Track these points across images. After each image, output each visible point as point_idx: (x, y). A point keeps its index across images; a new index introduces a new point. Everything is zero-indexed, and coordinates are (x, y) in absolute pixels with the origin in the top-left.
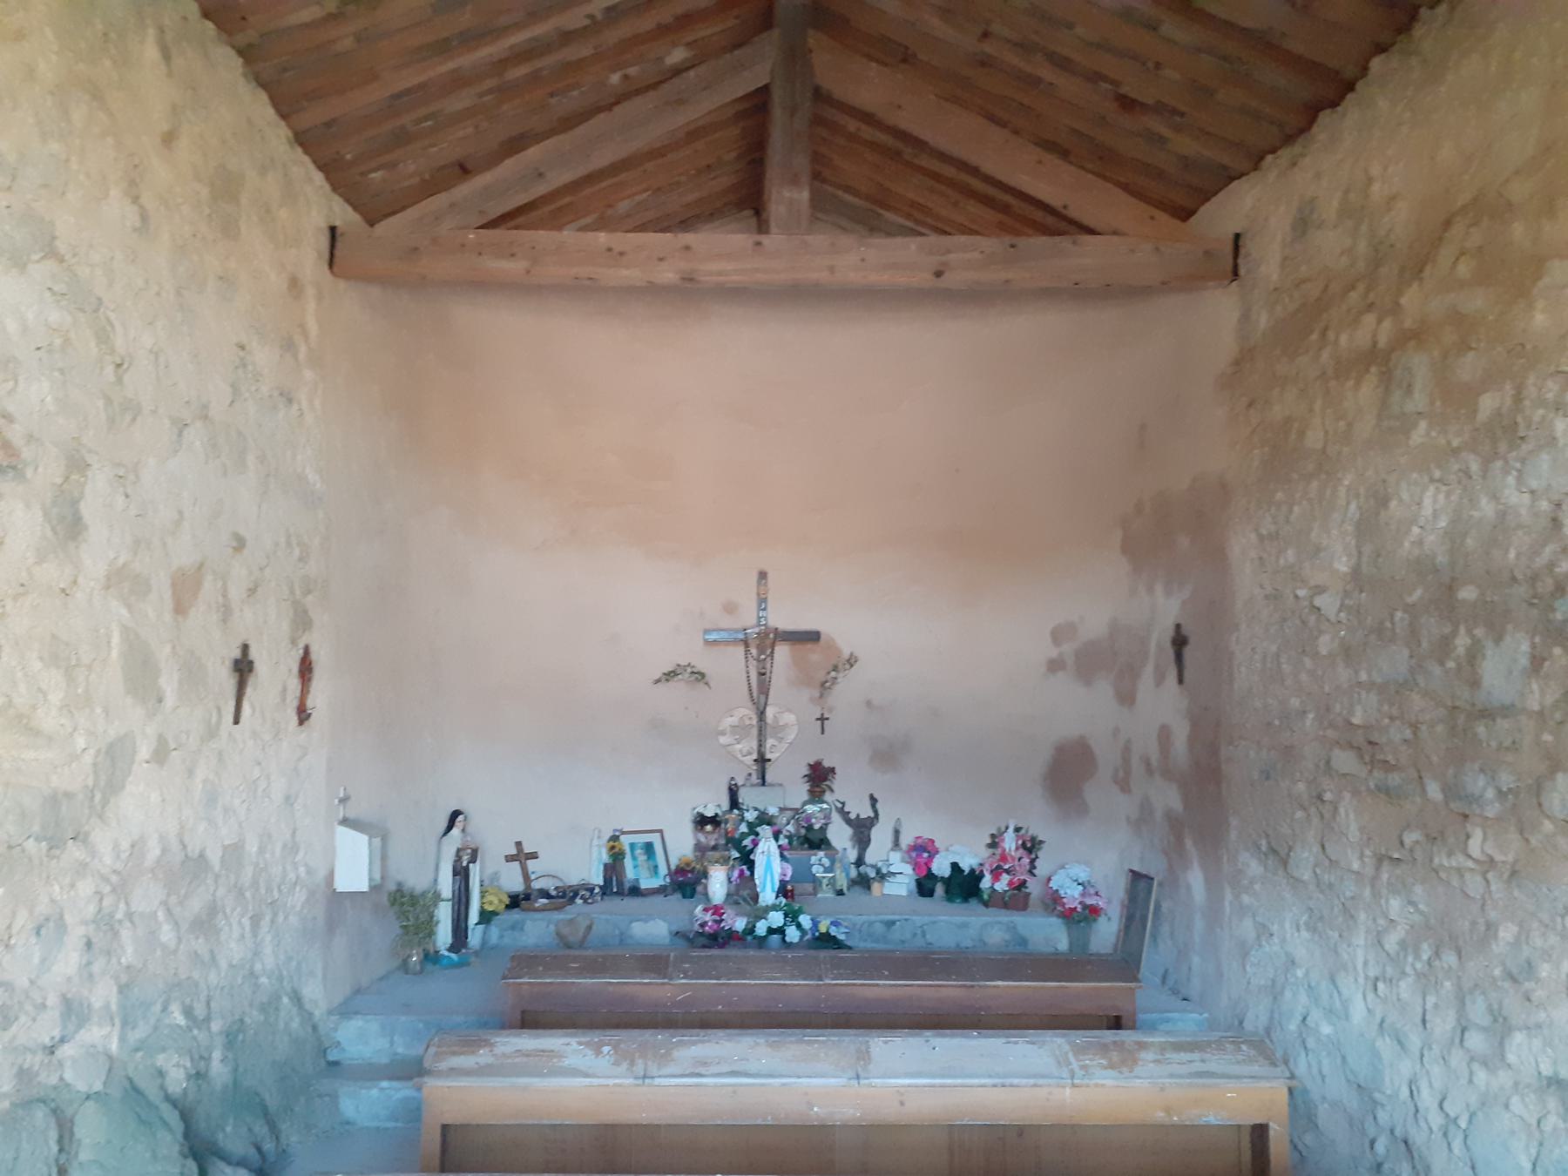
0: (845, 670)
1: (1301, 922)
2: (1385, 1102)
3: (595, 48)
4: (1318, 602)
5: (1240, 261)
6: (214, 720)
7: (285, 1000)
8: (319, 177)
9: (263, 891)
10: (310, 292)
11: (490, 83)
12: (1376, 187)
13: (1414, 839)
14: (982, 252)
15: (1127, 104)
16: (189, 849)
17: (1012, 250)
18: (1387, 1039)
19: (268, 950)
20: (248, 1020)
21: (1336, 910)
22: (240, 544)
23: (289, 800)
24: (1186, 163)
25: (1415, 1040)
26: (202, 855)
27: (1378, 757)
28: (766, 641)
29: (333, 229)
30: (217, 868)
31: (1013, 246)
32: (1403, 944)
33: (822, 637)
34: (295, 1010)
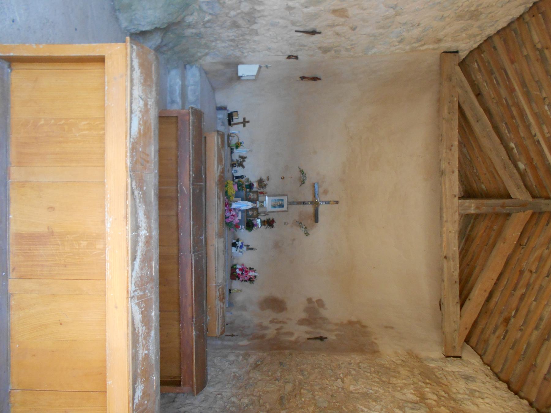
0: (305, 231)
1: (236, 374)
2: (184, 396)
3: (524, 137)
4: (339, 380)
5: (452, 358)
6: (298, 24)
7: (207, 51)
8: (476, 46)
9: (242, 42)
10: (436, 46)
11: (510, 102)
12: (481, 400)
13: (267, 406)
14: (453, 272)
15: (507, 321)
16: (258, 19)
17: (454, 282)
18: (204, 398)
19: (224, 45)
20: (203, 40)
21: (241, 384)
22: (354, 29)
23: (269, 49)
24: (486, 342)
25: (204, 405)
26: (255, 23)
27: (291, 397)
28: (315, 204)
29: (457, 52)
30: (251, 28)
31: (456, 282)
32: (234, 403)
33: (317, 223)
34: (203, 54)
